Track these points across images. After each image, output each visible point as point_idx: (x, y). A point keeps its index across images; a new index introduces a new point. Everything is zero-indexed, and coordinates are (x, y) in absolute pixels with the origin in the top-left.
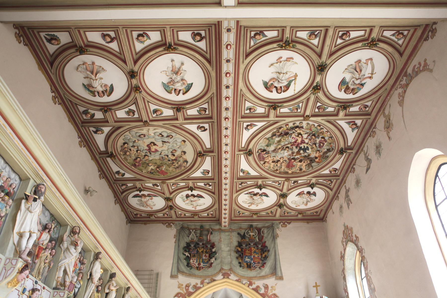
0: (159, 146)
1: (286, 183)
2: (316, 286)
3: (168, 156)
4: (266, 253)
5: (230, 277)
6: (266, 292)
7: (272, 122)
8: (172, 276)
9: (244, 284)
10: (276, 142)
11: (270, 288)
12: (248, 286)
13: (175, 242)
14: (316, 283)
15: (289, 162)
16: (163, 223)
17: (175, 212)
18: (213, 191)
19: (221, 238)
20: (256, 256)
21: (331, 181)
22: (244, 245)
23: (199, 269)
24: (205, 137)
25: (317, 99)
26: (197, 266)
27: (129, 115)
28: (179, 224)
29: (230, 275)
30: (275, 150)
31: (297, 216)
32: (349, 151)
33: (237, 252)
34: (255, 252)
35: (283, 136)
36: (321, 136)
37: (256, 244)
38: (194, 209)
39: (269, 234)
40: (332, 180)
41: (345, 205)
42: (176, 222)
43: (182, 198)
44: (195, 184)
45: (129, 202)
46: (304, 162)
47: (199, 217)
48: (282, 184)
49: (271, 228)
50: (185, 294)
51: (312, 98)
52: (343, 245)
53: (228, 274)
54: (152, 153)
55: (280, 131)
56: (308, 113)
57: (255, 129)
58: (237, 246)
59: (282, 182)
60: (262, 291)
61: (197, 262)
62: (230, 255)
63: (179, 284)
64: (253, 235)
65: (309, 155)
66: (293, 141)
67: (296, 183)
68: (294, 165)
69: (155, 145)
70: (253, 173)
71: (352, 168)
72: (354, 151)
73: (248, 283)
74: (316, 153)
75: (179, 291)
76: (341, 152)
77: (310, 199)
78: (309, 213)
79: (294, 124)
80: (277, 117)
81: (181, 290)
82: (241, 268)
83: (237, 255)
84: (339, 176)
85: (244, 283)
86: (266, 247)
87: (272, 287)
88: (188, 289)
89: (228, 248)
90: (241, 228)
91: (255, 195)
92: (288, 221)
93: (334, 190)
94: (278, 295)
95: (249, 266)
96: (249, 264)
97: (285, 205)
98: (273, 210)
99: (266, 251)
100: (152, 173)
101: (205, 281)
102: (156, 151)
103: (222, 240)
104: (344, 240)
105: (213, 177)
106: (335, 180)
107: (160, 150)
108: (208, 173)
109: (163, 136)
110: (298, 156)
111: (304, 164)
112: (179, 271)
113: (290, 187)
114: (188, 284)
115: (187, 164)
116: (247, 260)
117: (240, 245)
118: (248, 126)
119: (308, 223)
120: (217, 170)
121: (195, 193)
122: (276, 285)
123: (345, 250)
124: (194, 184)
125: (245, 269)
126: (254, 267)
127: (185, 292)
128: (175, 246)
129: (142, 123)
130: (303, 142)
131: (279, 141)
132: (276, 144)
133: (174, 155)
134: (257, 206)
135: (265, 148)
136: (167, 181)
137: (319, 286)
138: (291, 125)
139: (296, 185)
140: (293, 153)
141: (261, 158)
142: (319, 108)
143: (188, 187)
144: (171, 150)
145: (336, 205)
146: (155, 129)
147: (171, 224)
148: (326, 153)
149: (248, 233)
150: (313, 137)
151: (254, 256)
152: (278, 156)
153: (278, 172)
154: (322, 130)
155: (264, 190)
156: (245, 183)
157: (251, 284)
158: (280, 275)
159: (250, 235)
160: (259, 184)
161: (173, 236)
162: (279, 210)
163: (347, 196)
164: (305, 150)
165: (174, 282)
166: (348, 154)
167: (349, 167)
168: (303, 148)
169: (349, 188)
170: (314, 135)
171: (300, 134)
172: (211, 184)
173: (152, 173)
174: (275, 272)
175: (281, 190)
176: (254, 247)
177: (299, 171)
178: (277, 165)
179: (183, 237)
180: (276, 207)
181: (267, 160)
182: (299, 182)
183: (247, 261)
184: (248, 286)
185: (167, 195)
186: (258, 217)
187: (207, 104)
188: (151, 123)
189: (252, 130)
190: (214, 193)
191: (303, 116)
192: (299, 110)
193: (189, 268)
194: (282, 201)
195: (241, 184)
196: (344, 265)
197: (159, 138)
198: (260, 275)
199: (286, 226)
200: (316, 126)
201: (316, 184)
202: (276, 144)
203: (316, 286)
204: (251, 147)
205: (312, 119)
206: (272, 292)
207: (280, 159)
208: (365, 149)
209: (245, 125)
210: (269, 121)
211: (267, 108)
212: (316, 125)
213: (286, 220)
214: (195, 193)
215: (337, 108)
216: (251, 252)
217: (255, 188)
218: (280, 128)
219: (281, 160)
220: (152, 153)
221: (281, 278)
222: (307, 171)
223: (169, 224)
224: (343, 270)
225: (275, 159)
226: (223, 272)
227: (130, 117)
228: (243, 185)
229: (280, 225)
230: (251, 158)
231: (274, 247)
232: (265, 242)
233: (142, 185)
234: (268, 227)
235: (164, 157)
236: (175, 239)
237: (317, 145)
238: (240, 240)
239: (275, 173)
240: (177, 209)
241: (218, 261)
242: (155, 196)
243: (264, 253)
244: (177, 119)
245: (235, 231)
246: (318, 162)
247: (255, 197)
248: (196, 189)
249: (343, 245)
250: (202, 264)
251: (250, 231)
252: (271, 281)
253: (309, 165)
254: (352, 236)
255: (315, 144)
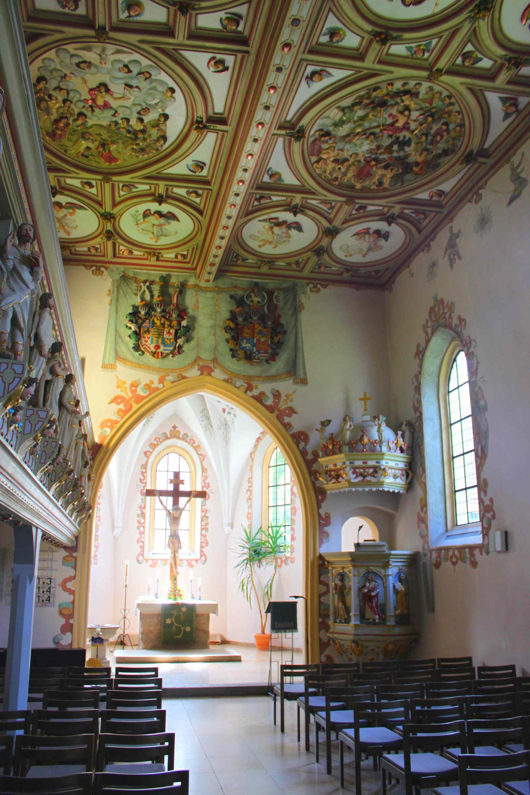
0: (116, 95)
1: (345, 208)
2: (364, 399)
3: (128, 120)
4: (280, 336)
5: (212, 374)
6: (276, 404)
7: (365, 72)
8: (105, 366)
9: (238, 388)
10: (356, 118)
11: (283, 397)
12: (246, 392)
13: (110, 304)
14: (365, 394)
15: (365, 166)
16: (85, 266)
17: (114, 245)
18: (201, 207)
19: (198, 302)
20: (262, 340)
21: (424, 214)
22: (240, 319)
23: (156, 355)
24: (219, 85)
25: (474, 36)
26: (154, 350)
27: (64, 7)
28: (118, 269)
29: (213, 371)
30: (348, 135)
31: (341, 274)
32: (481, 160)
33: (227, 329)
34: (260, 332)
35: (374, 108)
36: (443, 121)
37: (263, 319)
38: (152, 242)
39: (286, 302)
40: (427, 213)
41: (443, 262)
42: (111, 266)
43: (134, 216)
44: (170, 188)
45: (316, 233)
46: (392, 170)
47: (71, 253)
48: (335, 210)
49: (292, 292)
50: (131, 399)
51: (467, 27)
52: (426, 333)
53: (210, 368)
54: (97, 110)
55: (374, 94)
56: (442, 64)
57: (326, 82)
58: (228, 320)
59: (339, 204)
60: (270, 402)
61: (152, 342)
62: (215, 334)
63: (119, 381)
64: (259, 302)
65: (407, 157)
66: (390, 121)
67: (361, 211)
68: (371, 172)
69: (108, 91)
70: (289, 179)
71: (475, 193)
72: (490, 162)
73: (246, 385)
74: (421, 155)
75: (118, 392)
76: (469, 158)
77: (376, 244)
78: (363, 271)
79: (404, 85)
80: (380, 62)
81: (122, 391)
82: (235, 359)
83: (228, 336)
84: (442, 207)
85: (238, 385)
86: (282, 325)
87: (287, 396)
88: (135, 391)
89: (212, 322)
90: (236, 287)
91: (279, 224)
92: (323, 283)
93: (425, 233)
94: (296, 409)
95: (249, 357)
96: (248, 353)
97: (327, 252)
98: (305, 256)
99: (280, 332)
100: (87, 157)
101: (167, 378)
102: (106, 106)
103: (200, 305)
104: (430, 324)
105: (209, 178)
106: (433, 214)
107: (114, 104)
108: (202, 168)
109: (130, 71)
110: (386, 156)
111: (389, 176)
112: (118, 357)
113: (250, 208)
114: (135, 381)
115: (165, 143)
116: (245, 344)
117: (233, 317)
118: (313, 73)
119: (357, 289)
120: (222, 165)
121: (165, 208)
122: (294, 392)
123: (428, 341)
124: (167, 189)
125: (242, 362)
126: (258, 359)
127: (131, 395)
128: (110, 310)
129: (92, 33)
130: (406, 127)
131: (362, 119)
132: (355, 122)
133: (141, 120)
134: (275, 247)
135: (331, 129)
136: (114, 178)
137: (369, 399)
138: (398, 85)
139: (362, 214)
140: (379, 147)
141: (315, 149)
142: (466, 56)
143: (289, 205)
144: (139, 108)
145: (421, 261)
146: (118, 52)
147: (102, 269)
148: (439, 156)
149: (249, 296)
150: (430, 119)
151: (258, 341)
152: (348, 150)
153: (337, 183)
154: (450, 108)
155: (300, 218)
156: (266, 198)
157: (250, 388)
158: (302, 376)
159: (252, 301)
160: (293, 203)
161: (107, 291)
162: (314, 259)
163: (452, 245)
164: (404, 144)
165: (109, 375)
166: (476, 165)
167: (470, 191)
168: (401, 139)
169: (460, 232)
170: (432, 115)
171: (407, 108)
172: (200, 192)
173: (87, 157)
174: (294, 371)
175: (330, 221)
176: (259, 324)
177: (374, 187)
178: (339, 169)
179: (125, 296)
180: (309, 253)
181: (324, 156)
182: (370, 208)
183: (244, 348)
184: (246, 392)
185: (108, 207)
186: (270, 268)
187: (246, 5)
188: (112, 34)
189: (318, 86)
190: (201, 212)
191: (429, 69)
192: (426, 55)
193: (137, 354)
194: (325, 242)
195: (258, 200)
196: (421, 366)
197: (121, 75)
198: (268, 375)
199: (319, 291)
200: (443, 96)
201: (399, 217)
202: (355, 122)
203: (364, 399)
204: (304, 122)
205: (445, 78)
206: (286, 404)
207: (351, 156)
208: (516, 159)
209: (310, 69)
210: (358, 70)
211: (367, 37)
212: (445, 93)
213: (320, 281)
214: (165, 208)
215: (499, 61)
216: (253, 332)
217: (284, 210)
218: (375, 89)
219: (352, 160)
220: (97, 110)
221: (304, 382)
222: (391, 188)
223: (98, 269)
224: (418, 376)
225: (340, 157)
226: (201, 364)
227: (67, 10)
228: (263, 201)
229: (308, 289)
230: (296, 147)
231: (296, 327)
232: (280, 316)
233: (59, 181)
234: (286, 290)
235: (120, 122)
236: (110, 298)
237: (430, 138)
238: (232, 308)
239: (331, 185)
240: (120, 241)
241: (193, 343)
242: (81, 208)
243: (276, 335)
244: (171, 33)
245: (225, 292)
246: (417, 174)
247: (276, 230)
248: (170, 201)
249: (426, 333)
250: (162, 349)
251: (252, 294)
252: (285, 386)
253: (398, 179)
254: (450, 317)
255: (427, 135)
